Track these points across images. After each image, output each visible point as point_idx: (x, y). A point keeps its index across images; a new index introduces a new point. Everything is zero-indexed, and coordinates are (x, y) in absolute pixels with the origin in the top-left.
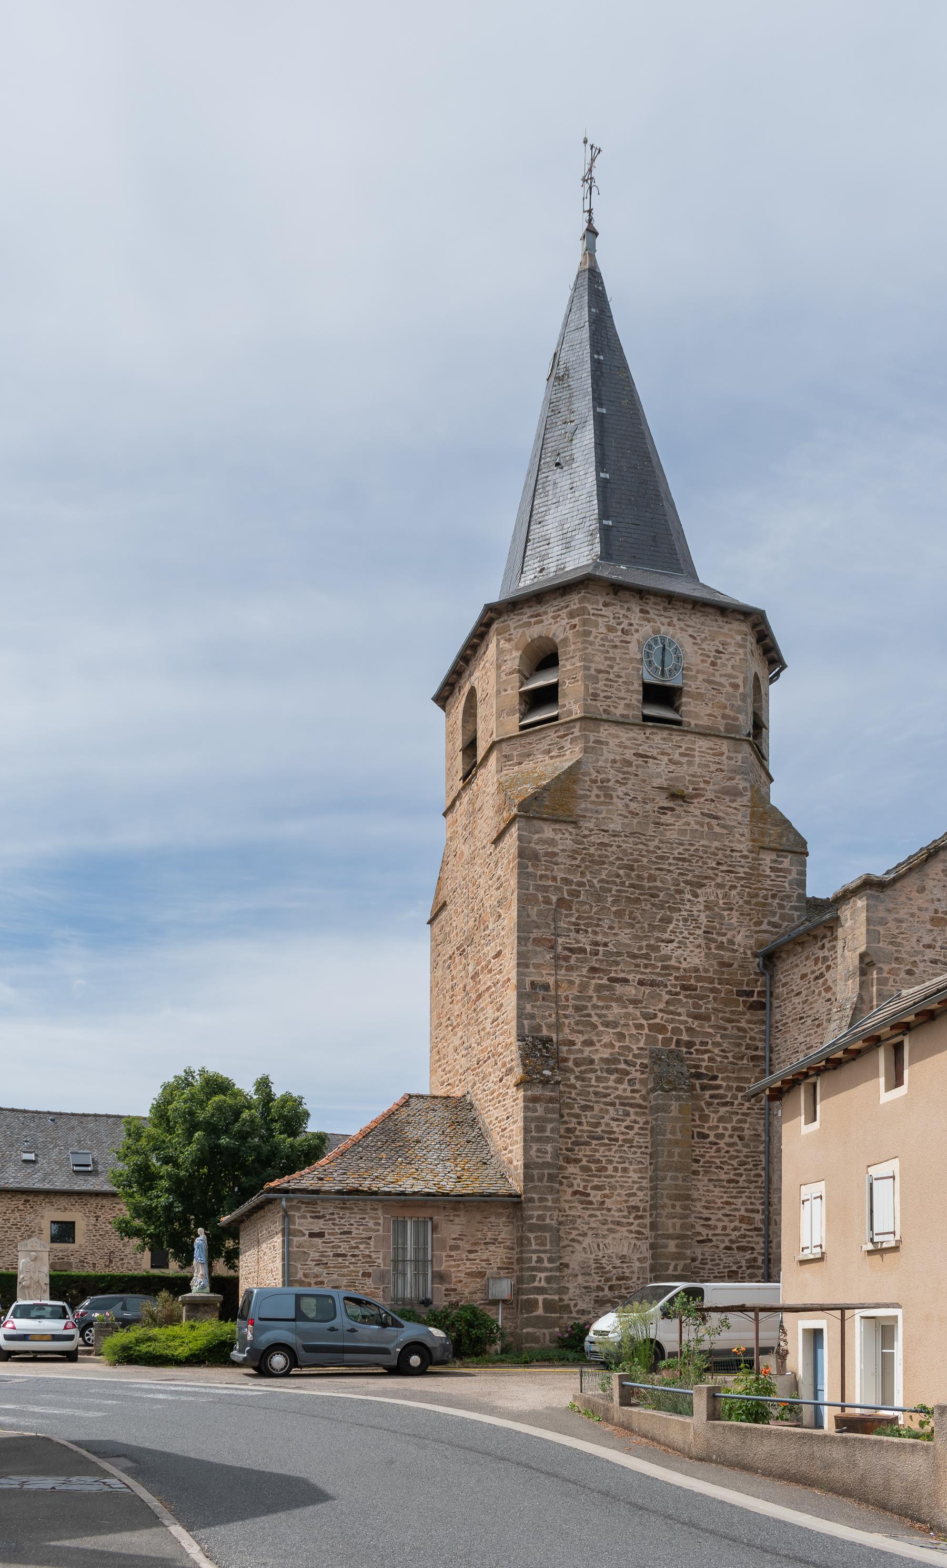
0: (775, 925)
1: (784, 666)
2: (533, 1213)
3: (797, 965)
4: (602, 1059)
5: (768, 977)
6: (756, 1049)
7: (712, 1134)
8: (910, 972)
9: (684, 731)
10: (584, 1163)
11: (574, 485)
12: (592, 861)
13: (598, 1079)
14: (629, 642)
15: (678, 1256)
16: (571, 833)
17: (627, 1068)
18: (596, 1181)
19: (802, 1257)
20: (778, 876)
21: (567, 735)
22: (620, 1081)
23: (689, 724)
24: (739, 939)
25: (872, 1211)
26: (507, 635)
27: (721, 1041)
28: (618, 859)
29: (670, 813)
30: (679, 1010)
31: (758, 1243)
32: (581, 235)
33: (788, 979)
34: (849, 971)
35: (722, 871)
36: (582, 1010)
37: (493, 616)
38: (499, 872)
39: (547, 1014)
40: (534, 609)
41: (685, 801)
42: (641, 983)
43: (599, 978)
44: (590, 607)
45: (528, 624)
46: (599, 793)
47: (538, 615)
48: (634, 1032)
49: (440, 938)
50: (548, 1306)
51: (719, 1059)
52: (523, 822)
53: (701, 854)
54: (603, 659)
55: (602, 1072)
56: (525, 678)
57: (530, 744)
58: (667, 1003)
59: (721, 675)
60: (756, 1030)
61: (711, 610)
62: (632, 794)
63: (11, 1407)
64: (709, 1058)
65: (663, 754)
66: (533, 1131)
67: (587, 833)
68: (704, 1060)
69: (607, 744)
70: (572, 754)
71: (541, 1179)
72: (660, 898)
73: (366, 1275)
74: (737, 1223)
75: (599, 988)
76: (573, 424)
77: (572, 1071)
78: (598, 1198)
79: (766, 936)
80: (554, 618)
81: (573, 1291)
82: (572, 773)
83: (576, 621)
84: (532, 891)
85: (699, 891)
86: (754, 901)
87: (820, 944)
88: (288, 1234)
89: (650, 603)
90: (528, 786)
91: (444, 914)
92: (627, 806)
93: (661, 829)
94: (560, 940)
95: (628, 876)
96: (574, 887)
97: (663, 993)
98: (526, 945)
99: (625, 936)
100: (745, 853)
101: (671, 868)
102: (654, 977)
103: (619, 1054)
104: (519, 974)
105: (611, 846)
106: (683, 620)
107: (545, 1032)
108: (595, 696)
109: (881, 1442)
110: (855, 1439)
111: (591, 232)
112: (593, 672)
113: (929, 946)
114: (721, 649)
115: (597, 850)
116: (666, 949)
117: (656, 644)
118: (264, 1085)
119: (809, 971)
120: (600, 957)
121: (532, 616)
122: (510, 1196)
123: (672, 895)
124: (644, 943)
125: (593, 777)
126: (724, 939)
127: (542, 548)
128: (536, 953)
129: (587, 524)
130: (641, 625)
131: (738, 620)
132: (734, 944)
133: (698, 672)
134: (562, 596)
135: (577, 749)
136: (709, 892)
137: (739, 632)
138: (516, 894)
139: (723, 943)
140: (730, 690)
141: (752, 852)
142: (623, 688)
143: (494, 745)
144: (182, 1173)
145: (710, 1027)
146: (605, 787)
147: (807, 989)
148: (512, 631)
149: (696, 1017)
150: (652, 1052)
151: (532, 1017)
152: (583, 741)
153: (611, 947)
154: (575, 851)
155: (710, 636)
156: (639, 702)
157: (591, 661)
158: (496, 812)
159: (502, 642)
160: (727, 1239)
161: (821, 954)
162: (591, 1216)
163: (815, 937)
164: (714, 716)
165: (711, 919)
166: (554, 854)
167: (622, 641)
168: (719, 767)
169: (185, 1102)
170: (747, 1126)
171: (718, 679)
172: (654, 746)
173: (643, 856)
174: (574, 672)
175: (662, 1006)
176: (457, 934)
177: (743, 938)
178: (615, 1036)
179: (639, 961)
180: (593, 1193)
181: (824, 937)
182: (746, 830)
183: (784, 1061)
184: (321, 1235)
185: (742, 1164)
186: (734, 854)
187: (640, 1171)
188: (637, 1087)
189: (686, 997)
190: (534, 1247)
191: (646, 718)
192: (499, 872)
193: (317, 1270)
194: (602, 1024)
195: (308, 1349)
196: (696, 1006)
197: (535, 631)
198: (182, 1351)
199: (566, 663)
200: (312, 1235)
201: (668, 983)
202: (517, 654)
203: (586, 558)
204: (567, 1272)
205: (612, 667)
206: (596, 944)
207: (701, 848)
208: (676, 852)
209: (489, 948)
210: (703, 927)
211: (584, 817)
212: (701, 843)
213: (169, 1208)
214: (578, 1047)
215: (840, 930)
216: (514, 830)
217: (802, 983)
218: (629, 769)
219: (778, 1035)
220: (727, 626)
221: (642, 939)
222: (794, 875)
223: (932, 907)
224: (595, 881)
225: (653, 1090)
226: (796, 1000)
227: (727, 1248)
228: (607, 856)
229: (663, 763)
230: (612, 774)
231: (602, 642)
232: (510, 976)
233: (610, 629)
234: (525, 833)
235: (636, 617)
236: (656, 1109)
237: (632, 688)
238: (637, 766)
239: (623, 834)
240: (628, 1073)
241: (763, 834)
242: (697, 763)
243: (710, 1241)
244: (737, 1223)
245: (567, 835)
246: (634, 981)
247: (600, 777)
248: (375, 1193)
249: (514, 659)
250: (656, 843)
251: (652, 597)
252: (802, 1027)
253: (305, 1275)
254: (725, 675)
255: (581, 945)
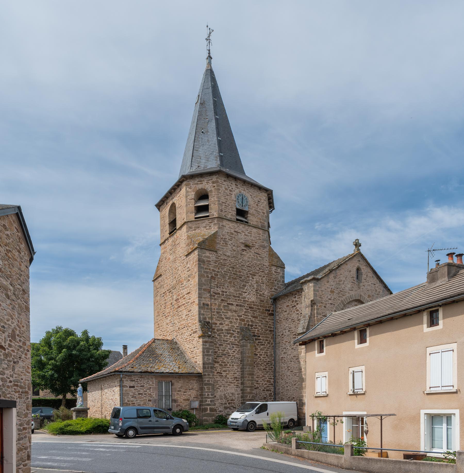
0: (276, 290)
1: (274, 209)
2: (206, 379)
4: (225, 329)
6: (271, 328)
7: (259, 354)
8: (325, 307)
10: (220, 363)
13: (224, 336)
15: (250, 393)
18: (224, 369)
19: (317, 396)
22: (231, 337)
24: (266, 293)
25: (353, 382)
26: (189, 186)
28: (230, 265)
31: (272, 388)
37: (184, 179)
38: (188, 266)
42: (237, 305)
47: (201, 181)
49: (159, 286)
50: (211, 410)
56: (196, 202)
62: (233, 244)
63: (44, 457)
65: (243, 232)
66: (205, 352)
67: (220, 255)
70: (214, 229)
71: (208, 368)
73: (149, 400)
74: (266, 382)
75: (224, 306)
78: (225, 374)
79: (274, 293)
80: (207, 183)
81: (217, 405)
82: (215, 235)
83: (215, 185)
86: (270, 281)
87: (294, 296)
88: (121, 386)
91: (160, 279)
92: (232, 248)
94: (212, 290)
95: (233, 270)
99: (232, 290)
104: (199, 300)
107: (207, 320)
108: (222, 211)
109: (432, 464)
110: (420, 463)
111: (210, 57)
113: (330, 299)
116: (245, 295)
118: (85, 333)
120: (224, 296)
122: (198, 373)
124: (238, 293)
126: (261, 293)
128: (204, 294)
136: (256, 278)
137: (265, 196)
138: (197, 273)
140: (262, 214)
143: (185, 223)
144: (58, 363)
149: (254, 317)
151: (203, 315)
153: (228, 293)
159: (188, 188)
160: (263, 387)
161: (294, 299)
162: (223, 380)
165: (258, 286)
166: (210, 261)
169: (58, 338)
170: (268, 352)
171: (259, 210)
175: (243, 313)
176: (167, 286)
177: (267, 293)
178: (229, 322)
180: (223, 373)
181: (296, 294)
184: (133, 387)
185: (267, 364)
187: (237, 366)
188: (236, 339)
189: (251, 310)
190: (206, 391)
191: (237, 220)
192: (188, 266)
193: (132, 399)
195: (142, 428)
196: (254, 314)
197: (200, 186)
198: (83, 429)
200: (130, 387)
202: (194, 193)
204: (216, 398)
206: (223, 292)
213: (52, 376)
214: (218, 325)
215: (303, 292)
216: (196, 252)
222: (281, 275)
223: (331, 287)
225: (242, 340)
226: (285, 313)
227: (263, 390)
230: (227, 237)
233: (226, 189)
235: (234, 186)
236: (242, 346)
240: (233, 334)
243: (258, 388)
244: (266, 382)
247: (224, 237)
248: (153, 373)
249: (192, 195)
250: (241, 260)
253: (128, 401)
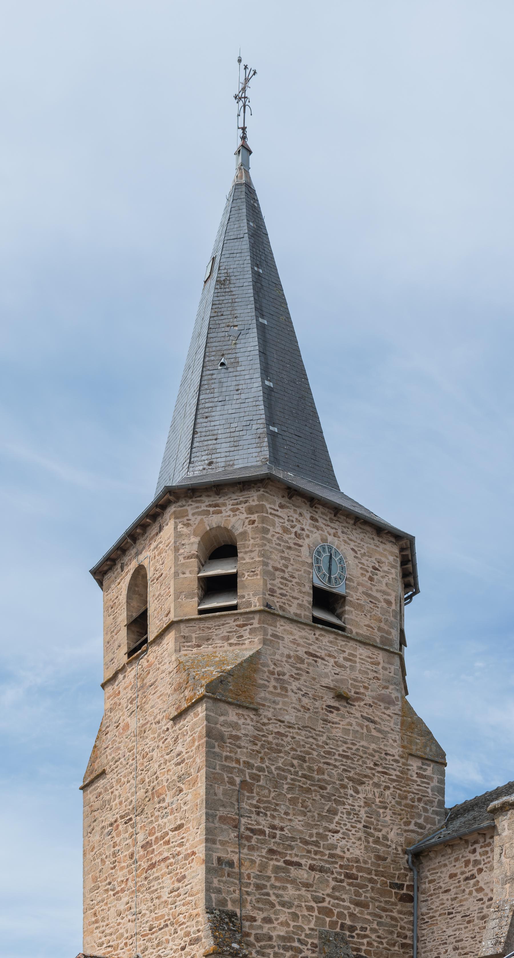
0: (420, 826)
1: (417, 592)
3: (445, 865)
4: (279, 936)
5: (416, 873)
6: (406, 937)
9: (347, 637)
11: (240, 387)
12: (270, 749)
14: (301, 546)
16: (252, 720)
17: (300, 946)
20: (423, 782)
21: (246, 625)
23: (351, 632)
24: (391, 835)
26: (185, 519)
27: (377, 927)
28: (293, 749)
29: (335, 712)
30: (344, 896)
32: (235, 149)
33: (435, 877)
34: (506, 876)
35: (378, 772)
36: (262, 889)
37: (170, 498)
38: (179, 748)
39: (232, 889)
40: (212, 499)
41: (348, 703)
42: (312, 868)
43: (277, 860)
44: (268, 506)
45: (207, 513)
46: (276, 684)
47: (216, 505)
48: (306, 913)
51: (375, 944)
52: (210, 703)
53: (361, 753)
54: (279, 558)
55: (279, 949)
56: (202, 565)
57: (210, 628)
58: (333, 888)
59: (377, 591)
60: (406, 920)
61: (368, 529)
62: (304, 689)
64: (368, 942)
65: (330, 656)
67: (265, 721)
68: (363, 944)
69: (283, 639)
70: (251, 645)
72: (328, 791)
75: (277, 869)
76: (236, 328)
77: (254, 945)
79: (413, 835)
80: (233, 510)
83: (254, 517)
84: (218, 771)
85: (359, 788)
86: (404, 802)
89: (319, 512)
90: (212, 669)
91: (101, 782)
92: (300, 700)
93: (328, 726)
94: (243, 820)
96: (254, 771)
97: (330, 879)
98: (213, 822)
99: (298, 822)
100: (397, 757)
101: (337, 764)
102: (323, 864)
103: (293, 933)
104: (208, 849)
105: (287, 736)
106: (346, 534)
107: (230, 907)
108: (272, 592)
111: (245, 150)
112: (270, 568)
114: (377, 566)
115: (274, 738)
116: (333, 839)
117: (324, 551)
119: (458, 871)
120: (277, 840)
121: (210, 506)
123: (337, 789)
124: (315, 831)
125: (271, 669)
126: (380, 835)
127: (210, 442)
128: (222, 830)
129: (255, 427)
130: (312, 532)
131: (391, 542)
132: (388, 840)
133: (359, 584)
134: (241, 491)
135: (256, 640)
136: (367, 790)
137: (392, 553)
139: (379, 838)
140: (385, 605)
141: (402, 757)
142: (296, 588)
145: (369, 914)
146: (281, 679)
147: (457, 887)
148: (190, 517)
149: (358, 904)
150: (321, 933)
152: (262, 633)
153: (286, 832)
154: (255, 737)
155: (368, 552)
156: (309, 604)
157: (269, 558)
158: (175, 690)
159: (180, 526)
161: (472, 857)
163: (467, 842)
164: (372, 628)
165: (369, 815)
166: (238, 738)
167: (295, 544)
168: (375, 675)
171: (374, 594)
172: (323, 647)
173: (313, 749)
174: (253, 566)
175: (329, 891)
176: (121, 803)
177: (394, 835)
179: (310, 847)
181: (476, 842)
182: (397, 737)
183: (431, 950)
186: (388, 757)
189: (349, 884)
191: (316, 620)
192: (179, 748)
194: (279, 903)
196: (358, 894)
197: (214, 521)
199: (245, 556)
201: (334, 870)
202: (195, 540)
203: (255, 459)
205: (287, 567)
206: (273, 827)
207: (361, 749)
208: (340, 749)
209: (165, 820)
210: (363, 821)
211: (264, 705)
212: (361, 744)
215: (496, 838)
217: (451, 881)
218: (302, 666)
219: (424, 926)
220: (382, 546)
221: (312, 827)
222: (435, 783)
224: (273, 768)
226: (445, 897)
228: (283, 746)
229: (330, 664)
231: (278, 542)
232: (195, 850)
233: (286, 530)
234: (212, 714)
237: (304, 590)
238: (309, 664)
239: (296, 726)
241: (411, 742)
242: (358, 668)
245: (249, 721)
246: (306, 865)
247: (278, 669)
249: (192, 544)
250: (324, 738)
251: (320, 507)
252: (451, 921)
254: (380, 591)
255: (261, 827)
